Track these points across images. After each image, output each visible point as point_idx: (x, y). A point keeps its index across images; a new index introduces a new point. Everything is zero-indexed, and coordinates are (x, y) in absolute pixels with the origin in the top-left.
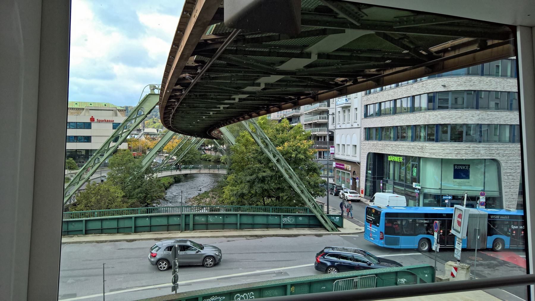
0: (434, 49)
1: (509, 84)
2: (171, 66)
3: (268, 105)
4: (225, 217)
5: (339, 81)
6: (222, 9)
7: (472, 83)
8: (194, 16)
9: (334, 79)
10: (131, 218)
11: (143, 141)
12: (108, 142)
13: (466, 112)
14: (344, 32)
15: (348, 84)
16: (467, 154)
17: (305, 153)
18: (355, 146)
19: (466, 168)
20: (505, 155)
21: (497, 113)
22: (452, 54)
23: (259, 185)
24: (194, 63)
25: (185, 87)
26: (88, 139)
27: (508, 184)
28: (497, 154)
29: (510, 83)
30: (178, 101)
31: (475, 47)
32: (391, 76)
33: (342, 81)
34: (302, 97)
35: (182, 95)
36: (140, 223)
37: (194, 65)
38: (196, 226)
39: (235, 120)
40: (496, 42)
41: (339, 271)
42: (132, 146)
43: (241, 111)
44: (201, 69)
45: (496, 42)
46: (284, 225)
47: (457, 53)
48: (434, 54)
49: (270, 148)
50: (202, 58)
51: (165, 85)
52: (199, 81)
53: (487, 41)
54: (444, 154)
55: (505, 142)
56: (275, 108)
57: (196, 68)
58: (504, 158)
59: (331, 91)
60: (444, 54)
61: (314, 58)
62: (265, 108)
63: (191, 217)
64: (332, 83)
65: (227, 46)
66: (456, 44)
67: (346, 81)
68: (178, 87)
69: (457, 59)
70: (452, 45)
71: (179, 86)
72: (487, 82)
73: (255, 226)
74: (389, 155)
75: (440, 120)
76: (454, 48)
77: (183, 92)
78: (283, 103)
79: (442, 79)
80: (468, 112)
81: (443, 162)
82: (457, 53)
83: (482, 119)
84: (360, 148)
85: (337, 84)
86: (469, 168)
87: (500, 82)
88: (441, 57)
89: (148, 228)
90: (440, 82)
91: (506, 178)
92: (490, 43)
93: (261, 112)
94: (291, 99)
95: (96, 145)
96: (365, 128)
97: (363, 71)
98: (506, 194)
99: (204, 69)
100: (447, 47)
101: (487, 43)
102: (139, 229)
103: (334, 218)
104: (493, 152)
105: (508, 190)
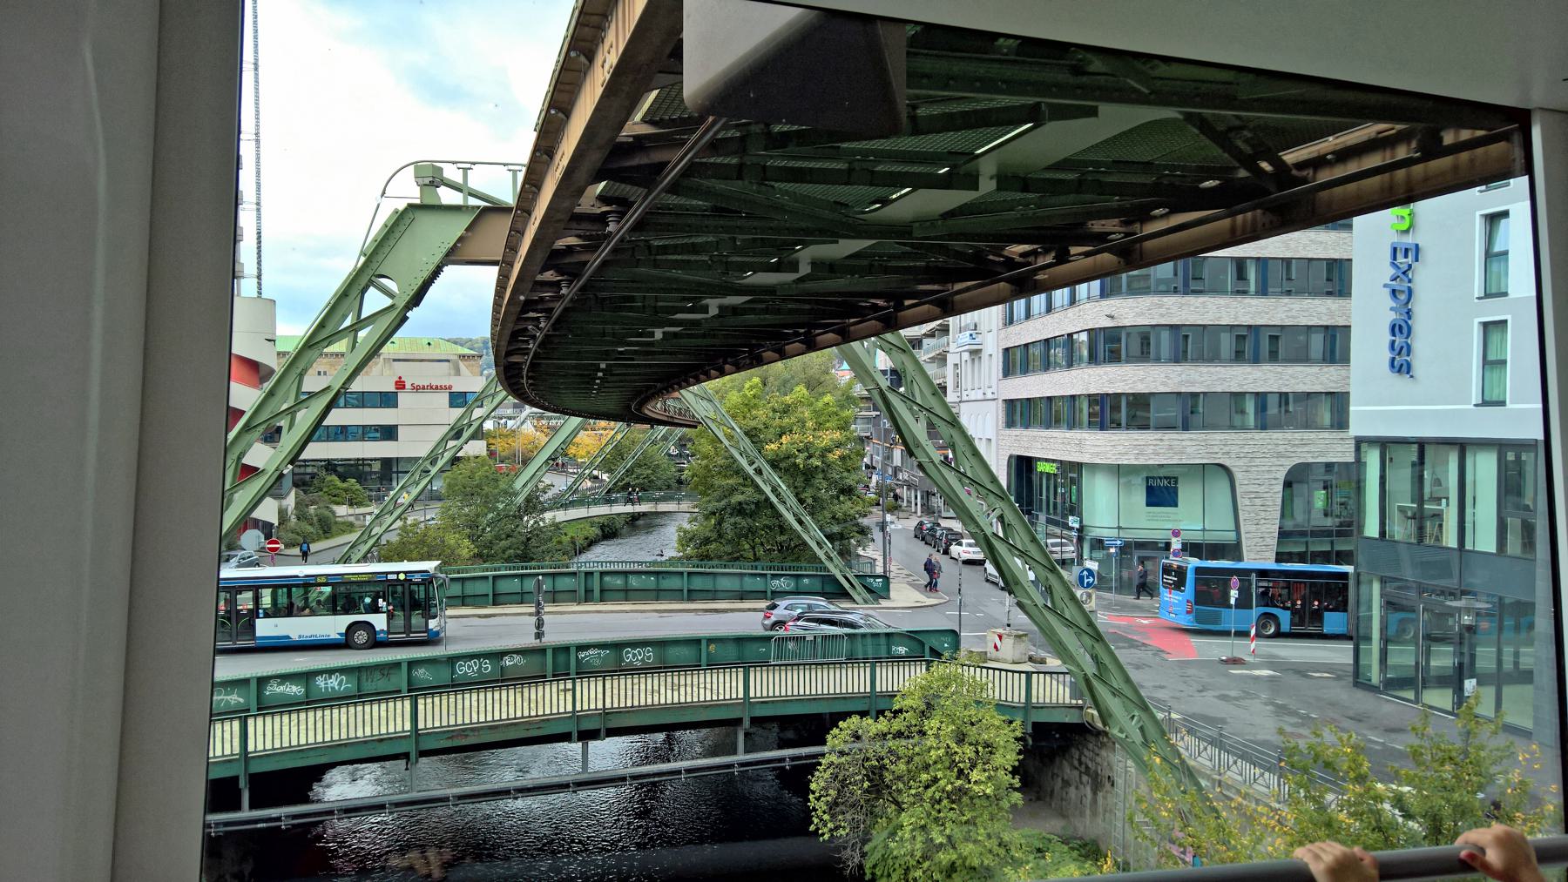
0: (1290, 157)
1: (1248, 309)
2: (530, 215)
4: (660, 577)
5: (1014, 253)
6: (682, 40)
7: (1162, 311)
8: (600, 63)
9: (1003, 248)
10: (486, 578)
11: (527, 436)
12: (444, 440)
13: (1153, 368)
15: (1041, 262)
16: (1158, 454)
18: (990, 440)
19: (1170, 483)
20: (1242, 455)
21: (1222, 369)
22: (1340, 172)
23: (732, 520)
24: (598, 204)
25: (569, 274)
26: (389, 433)
27: (1252, 515)
28: (1224, 453)
29: (1250, 306)
32: (1165, 238)
33: (1023, 255)
34: (907, 303)
35: (593, 243)
36: (504, 587)
37: (599, 211)
38: (607, 594)
39: (712, 372)
40: (1465, 135)
42: (499, 449)
44: (618, 222)
45: (1465, 135)
46: (773, 592)
47: (1352, 167)
48: (1294, 172)
50: (624, 189)
51: (510, 272)
53: (1443, 134)
54: (1114, 455)
55: (1322, 428)
56: (831, 336)
57: (601, 219)
58: (1241, 463)
59: (992, 283)
60: (1315, 173)
62: (800, 334)
63: (597, 576)
64: (997, 259)
65: (695, 156)
66: (1349, 143)
68: (549, 276)
69: (1352, 187)
70: (1338, 148)
71: (551, 272)
72: (1197, 307)
73: (720, 595)
74: (1040, 459)
75: (1106, 384)
76: (1344, 155)
78: (852, 320)
79: (1108, 302)
80: (1157, 368)
81: (1119, 471)
82: (1352, 167)
83: (1188, 382)
84: (998, 444)
85: (1010, 263)
86: (1176, 482)
87: (1227, 306)
88: (1030, 264)
89: (518, 598)
90: (1105, 309)
91: (1247, 502)
92: (1448, 138)
94: (875, 308)
95: (404, 447)
96: (1005, 401)
97: (1083, 224)
98: (1248, 535)
99: (624, 225)
100: (1322, 152)
101: (1441, 140)
102: (501, 599)
103: (872, 580)
104: (1216, 449)
105: (1253, 528)
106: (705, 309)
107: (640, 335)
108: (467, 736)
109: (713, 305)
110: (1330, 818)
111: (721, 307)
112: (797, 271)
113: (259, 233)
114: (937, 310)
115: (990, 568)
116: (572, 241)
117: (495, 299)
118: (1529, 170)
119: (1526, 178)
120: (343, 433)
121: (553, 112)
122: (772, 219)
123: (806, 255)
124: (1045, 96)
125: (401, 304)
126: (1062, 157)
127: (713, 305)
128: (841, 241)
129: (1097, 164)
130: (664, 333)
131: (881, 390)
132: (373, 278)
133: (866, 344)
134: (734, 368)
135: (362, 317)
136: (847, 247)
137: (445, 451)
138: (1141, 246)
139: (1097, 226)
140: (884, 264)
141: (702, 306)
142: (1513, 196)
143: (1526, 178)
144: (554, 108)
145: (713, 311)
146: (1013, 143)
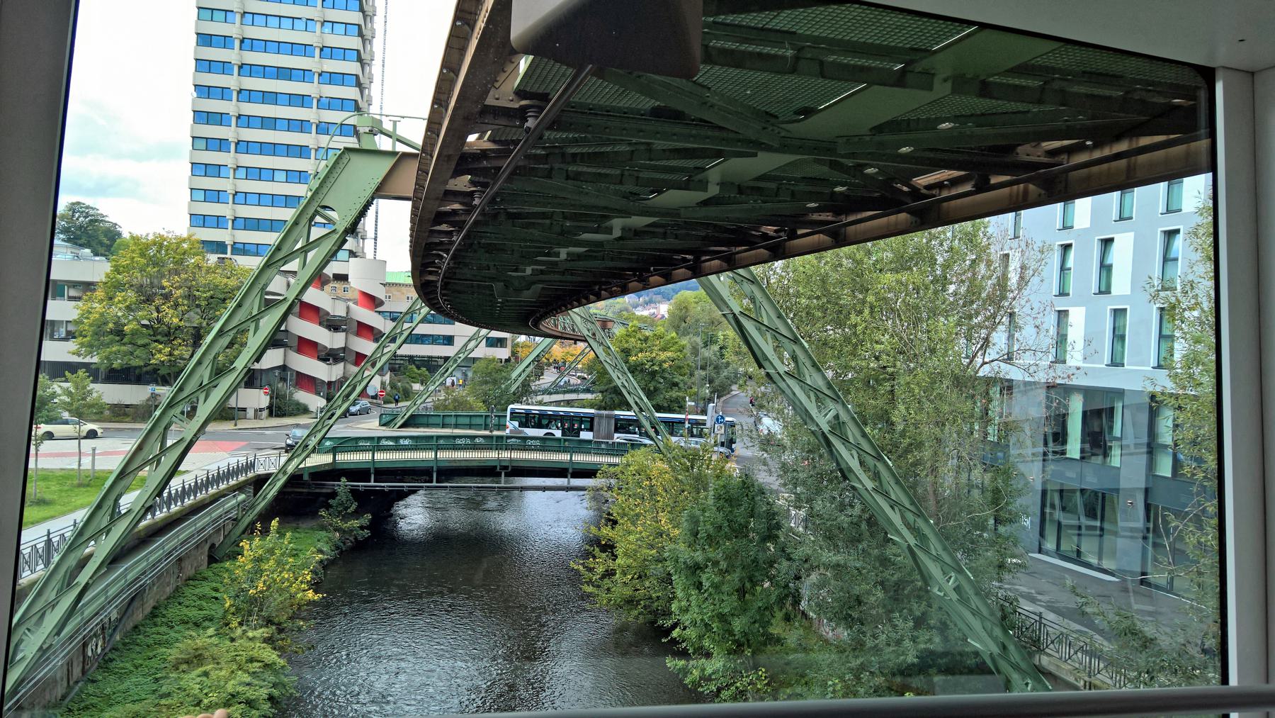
0: (922, 181)
3: (698, 253)
14: (755, 155)
17: (660, 365)
30: (459, 232)
31: (968, 187)
35: (470, 209)
37: (517, 106)
41: (528, 289)
43: (616, 268)
44: (537, 117)
49: (973, 604)
52: (521, 163)
56: (717, 262)
60: (1069, 158)
61: (713, 190)
67: (1070, 151)
77: (476, 202)
88: (935, 196)
92: (800, 232)
93: (652, 279)
94: (685, 260)
100: (942, 179)
107: (548, 255)
109: (617, 224)
112: (705, 190)
114: (725, 265)
116: (456, 206)
117: (412, 210)
118: (1213, 168)
119: (1210, 175)
120: (421, 339)
121: (436, 106)
122: (90, 556)
123: (716, 172)
125: (341, 229)
126: (889, 118)
127: (617, 224)
128: (760, 154)
129: (789, 179)
130: (533, 270)
131: (735, 315)
132: (319, 209)
133: (722, 279)
135: (311, 241)
136: (766, 162)
137: (382, 355)
138: (1067, 176)
139: (1026, 153)
140: (792, 188)
142: (1195, 189)
143: (1210, 175)
144: (437, 104)
146: (967, 41)
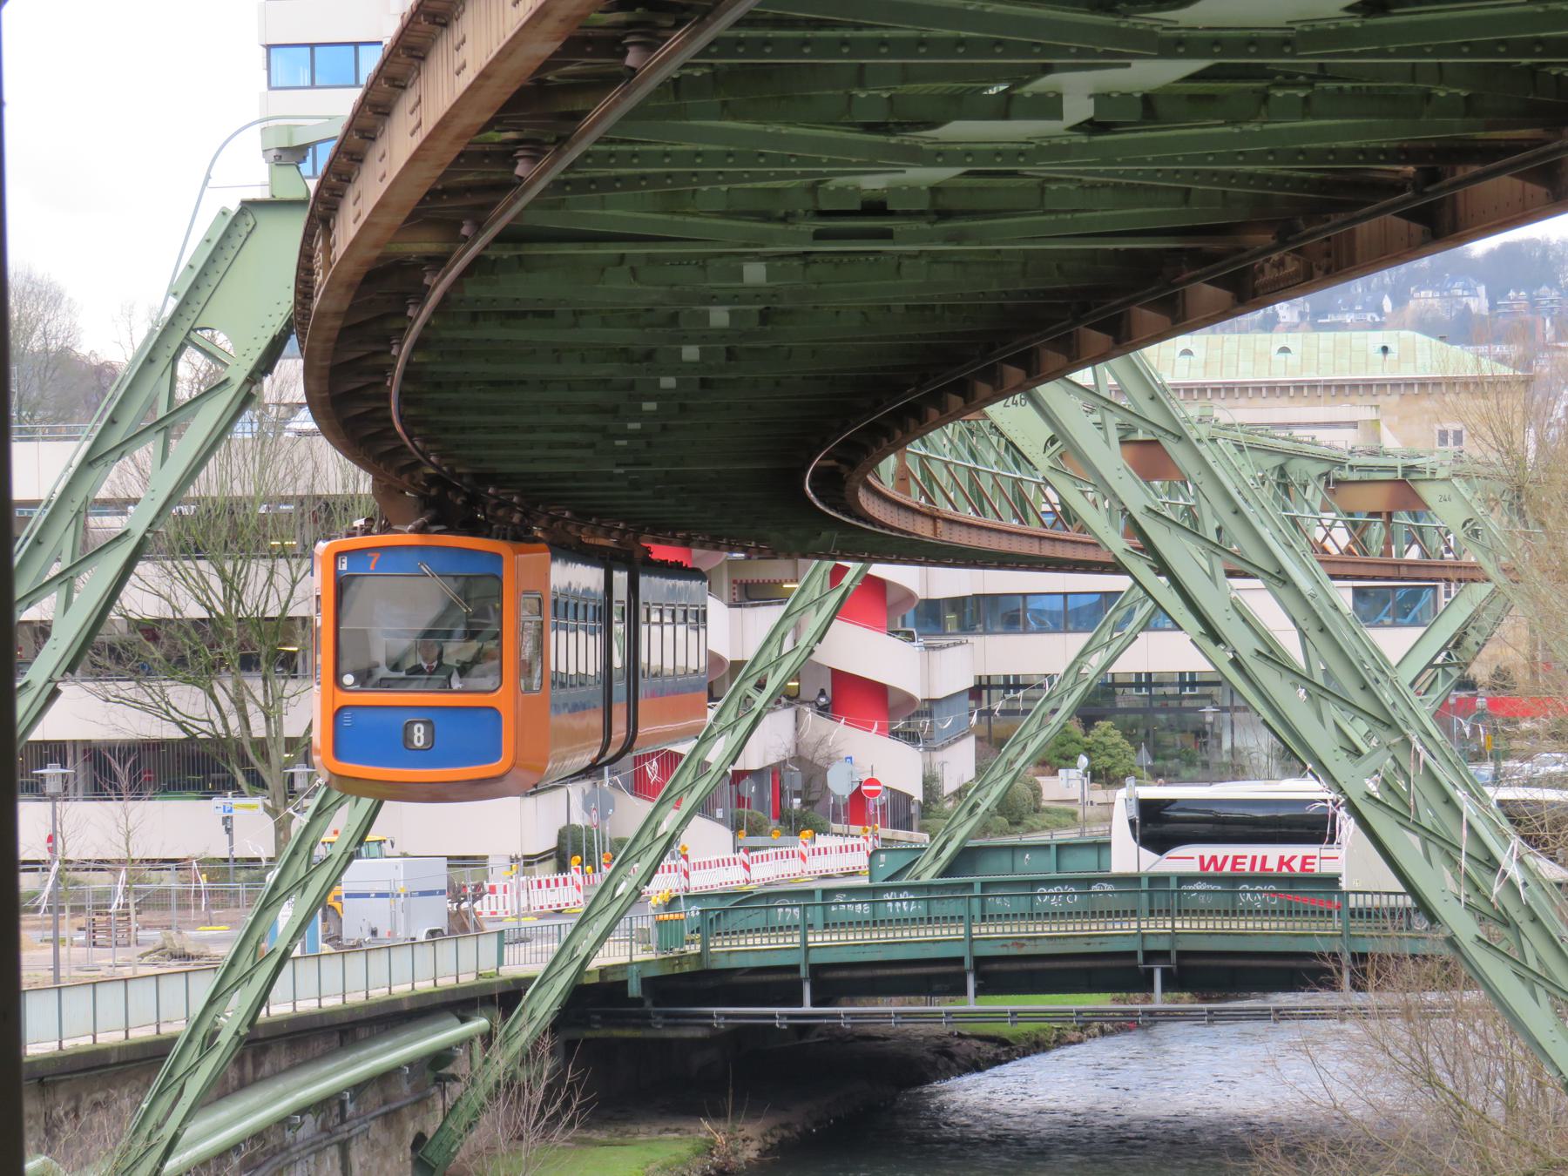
101: (620, 569)
106: (1050, 106)
108: (1023, 945)
110: (1455, 986)
111: (1101, 98)
113: (423, 894)
115: (1480, 782)
124: (794, 125)
134: (1224, 295)
141: (1039, 98)
145: (1079, 108)
